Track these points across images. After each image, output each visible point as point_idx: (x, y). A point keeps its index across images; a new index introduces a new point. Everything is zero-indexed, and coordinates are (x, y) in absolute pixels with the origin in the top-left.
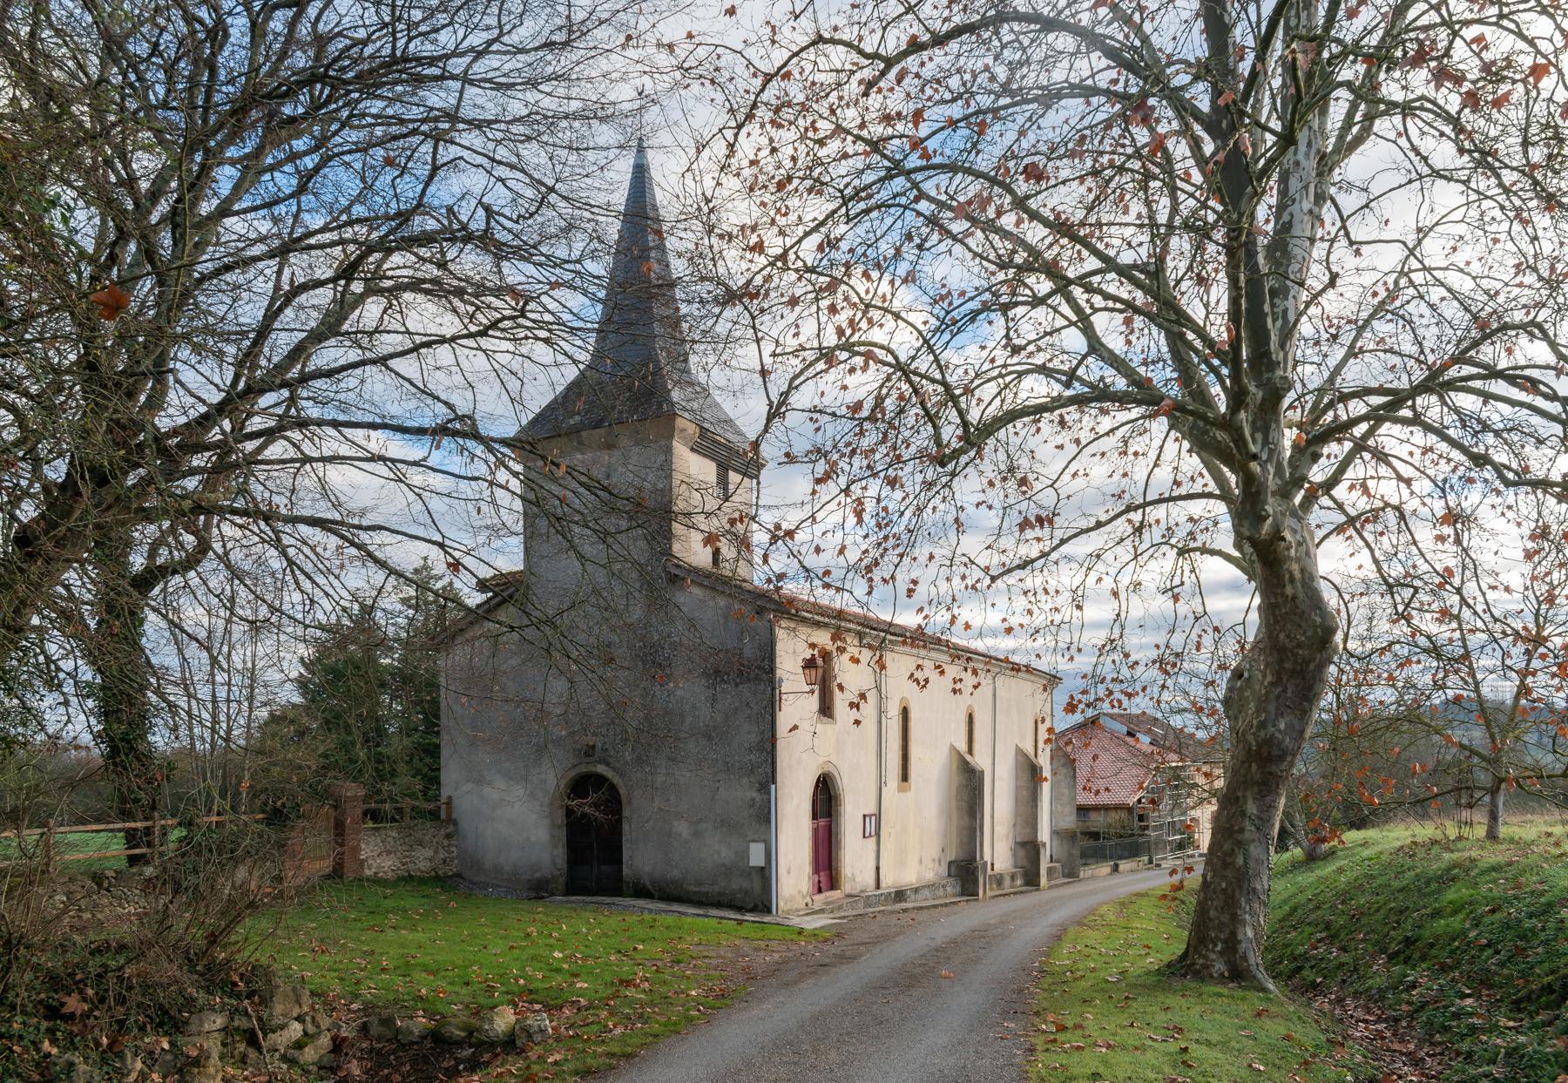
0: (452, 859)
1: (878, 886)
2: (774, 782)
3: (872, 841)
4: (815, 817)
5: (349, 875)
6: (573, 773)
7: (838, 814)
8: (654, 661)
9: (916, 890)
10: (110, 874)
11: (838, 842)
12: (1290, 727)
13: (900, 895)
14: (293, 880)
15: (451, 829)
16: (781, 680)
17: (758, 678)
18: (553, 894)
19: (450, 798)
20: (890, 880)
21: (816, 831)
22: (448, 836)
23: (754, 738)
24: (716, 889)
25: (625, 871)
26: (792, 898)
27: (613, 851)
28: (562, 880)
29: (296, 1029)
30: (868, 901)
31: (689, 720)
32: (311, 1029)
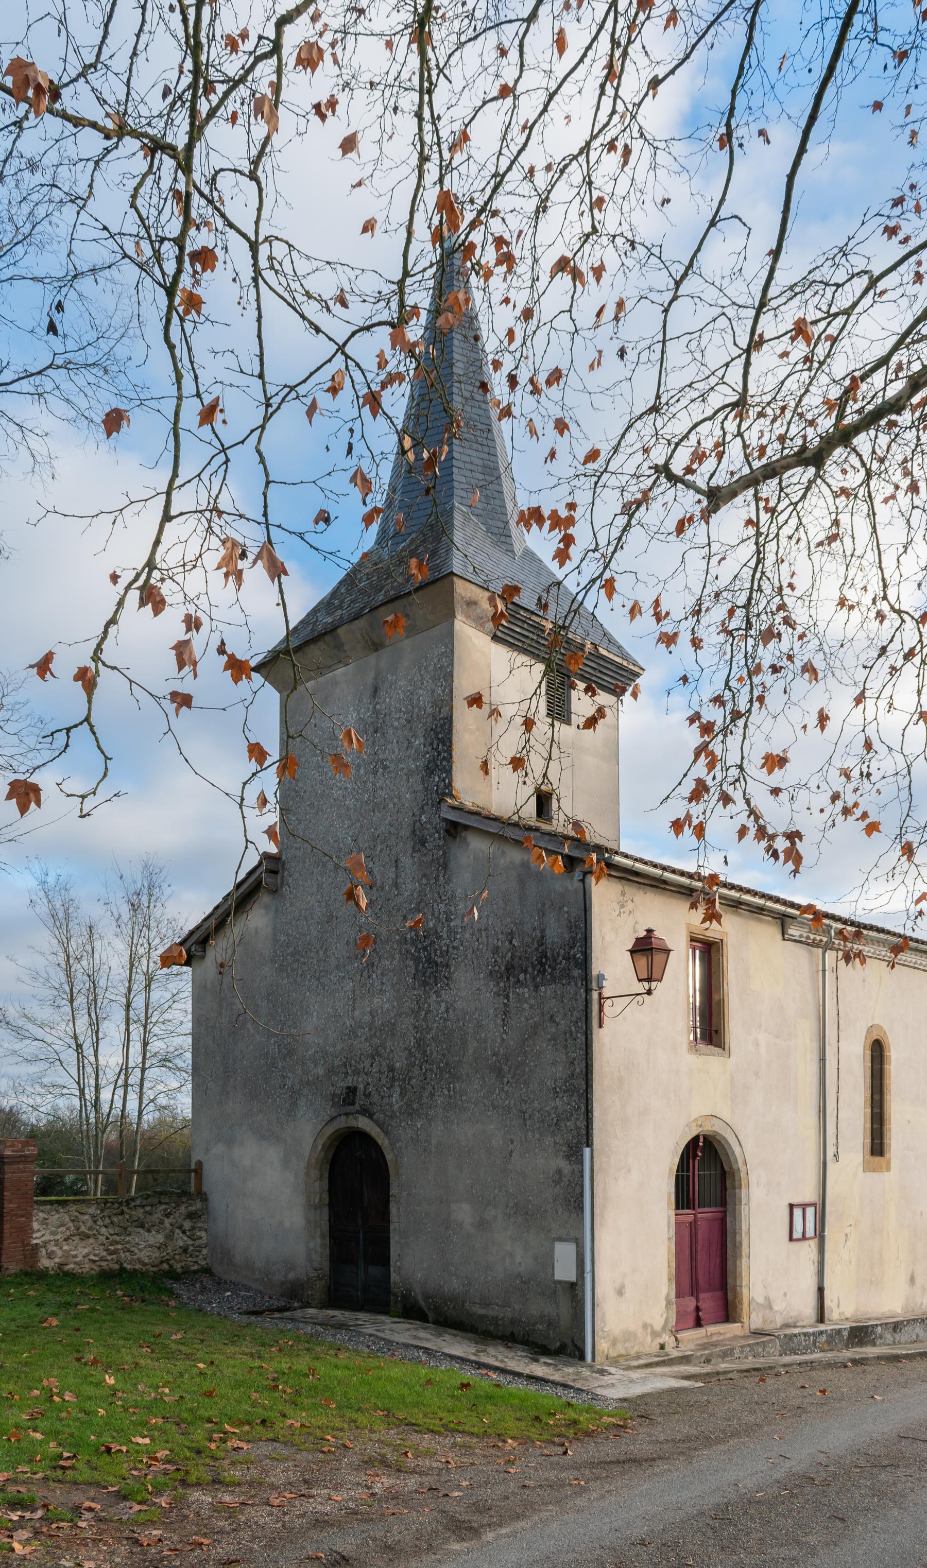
0: (199, 1248)
1: (821, 1318)
2: (589, 1144)
3: (809, 1249)
4: (677, 1208)
6: (330, 1130)
7: (737, 1201)
8: (429, 963)
9: (896, 1327)
11: (737, 1246)
13: (860, 1334)
15: (198, 1205)
16: (601, 977)
17: (566, 975)
18: (308, 1305)
19: (200, 1164)
20: (845, 1307)
21: (678, 1224)
22: (191, 1216)
23: (560, 1071)
24: (509, 1313)
25: (394, 1277)
26: (629, 1336)
28: (320, 1285)
30: (790, 1343)
31: (473, 1045)
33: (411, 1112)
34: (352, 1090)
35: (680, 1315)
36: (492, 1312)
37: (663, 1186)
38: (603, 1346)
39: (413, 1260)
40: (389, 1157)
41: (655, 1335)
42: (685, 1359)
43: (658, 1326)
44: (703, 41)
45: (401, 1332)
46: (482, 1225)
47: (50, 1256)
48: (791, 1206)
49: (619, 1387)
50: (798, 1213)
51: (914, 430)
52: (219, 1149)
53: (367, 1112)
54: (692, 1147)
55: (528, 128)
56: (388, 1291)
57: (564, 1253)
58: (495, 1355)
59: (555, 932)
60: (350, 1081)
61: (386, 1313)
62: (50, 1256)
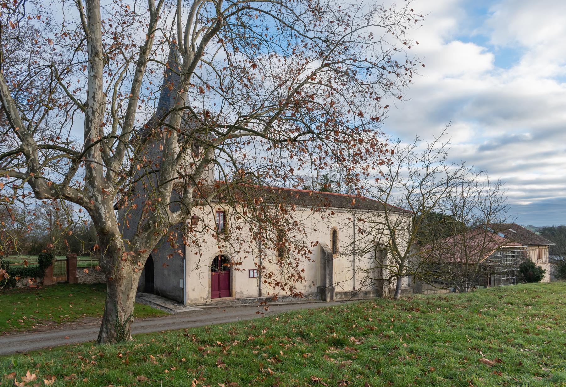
1: (260, 295)
5: (71, 282)
14: (47, 282)
26: (196, 299)
36: (170, 294)
38: (189, 302)
39: (158, 283)
43: (205, 297)
44: (261, 8)
46: (169, 275)
47: (81, 280)
48: (249, 270)
50: (251, 272)
51: (66, 141)
55: (197, 33)
57: (181, 281)
61: (153, 294)
62: (81, 280)
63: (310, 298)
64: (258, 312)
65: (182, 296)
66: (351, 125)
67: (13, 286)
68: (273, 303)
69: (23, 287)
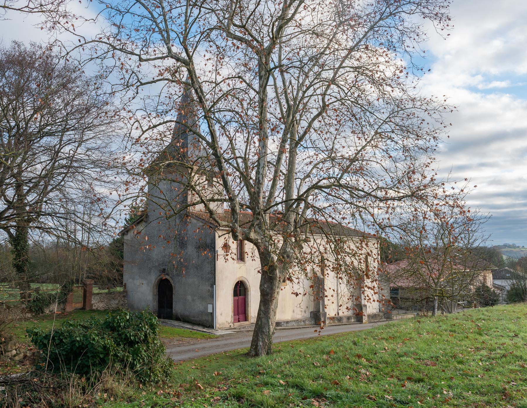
4: (234, 296)
5: (88, 308)
8: (183, 244)
9: (287, 322)
10: (12, 306)
11: (248, 304)
12: (268, 286)
14: (69, 309)
16: (217, 251)
19: (125, 284)
21: (234, 300)
23: (209, 269)
24: (198, 319)
25: (174, 311)
26: (223, 324)
27: (170, 305)
29: (14, 352)
32: (18, 352)
33: (178, 275)
34: (164, 269)
35: (234, 319)
37: (231, 292)
38: (218, 326)
39: (178, 308)
40: (173, 285)
41: (229, 323)
42: (235, 328)
43: (229, 322)
45: (176, 323)
46: (193, 300)
47: (95, 306)
49: (219, 333)
52: (131, 280)
53: (168, 274)
54: (238, 283)
56: (172, 314)
57: (210, 307)
58: (196, 327)
59: (209, 241)
60: (164, 267)
61: (172, 319)
63: (307, 322)
64: (316, 331)
65: (210, 320)
66: (138, 160)
67: (42, 313)
68: (280, 328)
69: (50, 313)
